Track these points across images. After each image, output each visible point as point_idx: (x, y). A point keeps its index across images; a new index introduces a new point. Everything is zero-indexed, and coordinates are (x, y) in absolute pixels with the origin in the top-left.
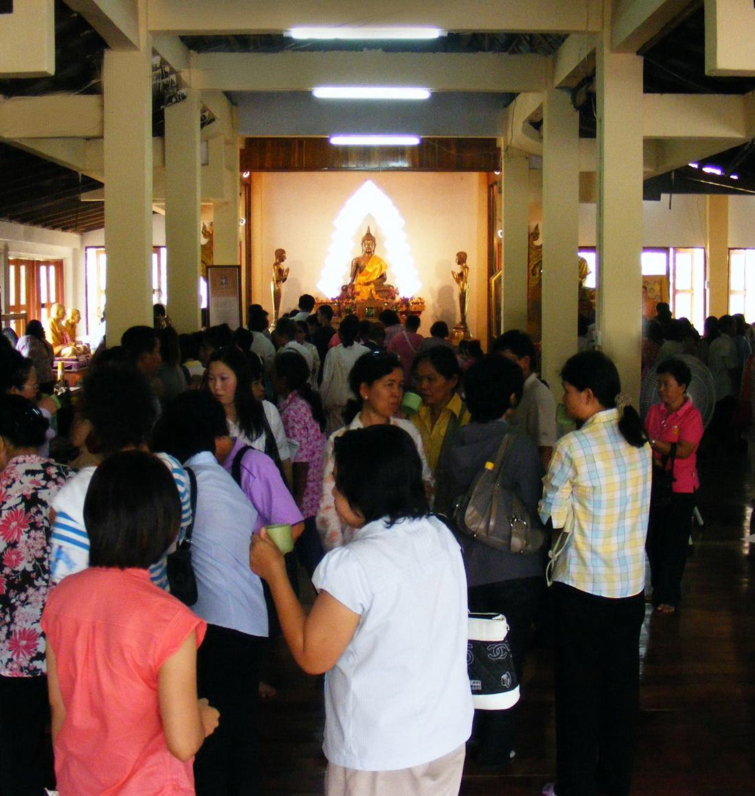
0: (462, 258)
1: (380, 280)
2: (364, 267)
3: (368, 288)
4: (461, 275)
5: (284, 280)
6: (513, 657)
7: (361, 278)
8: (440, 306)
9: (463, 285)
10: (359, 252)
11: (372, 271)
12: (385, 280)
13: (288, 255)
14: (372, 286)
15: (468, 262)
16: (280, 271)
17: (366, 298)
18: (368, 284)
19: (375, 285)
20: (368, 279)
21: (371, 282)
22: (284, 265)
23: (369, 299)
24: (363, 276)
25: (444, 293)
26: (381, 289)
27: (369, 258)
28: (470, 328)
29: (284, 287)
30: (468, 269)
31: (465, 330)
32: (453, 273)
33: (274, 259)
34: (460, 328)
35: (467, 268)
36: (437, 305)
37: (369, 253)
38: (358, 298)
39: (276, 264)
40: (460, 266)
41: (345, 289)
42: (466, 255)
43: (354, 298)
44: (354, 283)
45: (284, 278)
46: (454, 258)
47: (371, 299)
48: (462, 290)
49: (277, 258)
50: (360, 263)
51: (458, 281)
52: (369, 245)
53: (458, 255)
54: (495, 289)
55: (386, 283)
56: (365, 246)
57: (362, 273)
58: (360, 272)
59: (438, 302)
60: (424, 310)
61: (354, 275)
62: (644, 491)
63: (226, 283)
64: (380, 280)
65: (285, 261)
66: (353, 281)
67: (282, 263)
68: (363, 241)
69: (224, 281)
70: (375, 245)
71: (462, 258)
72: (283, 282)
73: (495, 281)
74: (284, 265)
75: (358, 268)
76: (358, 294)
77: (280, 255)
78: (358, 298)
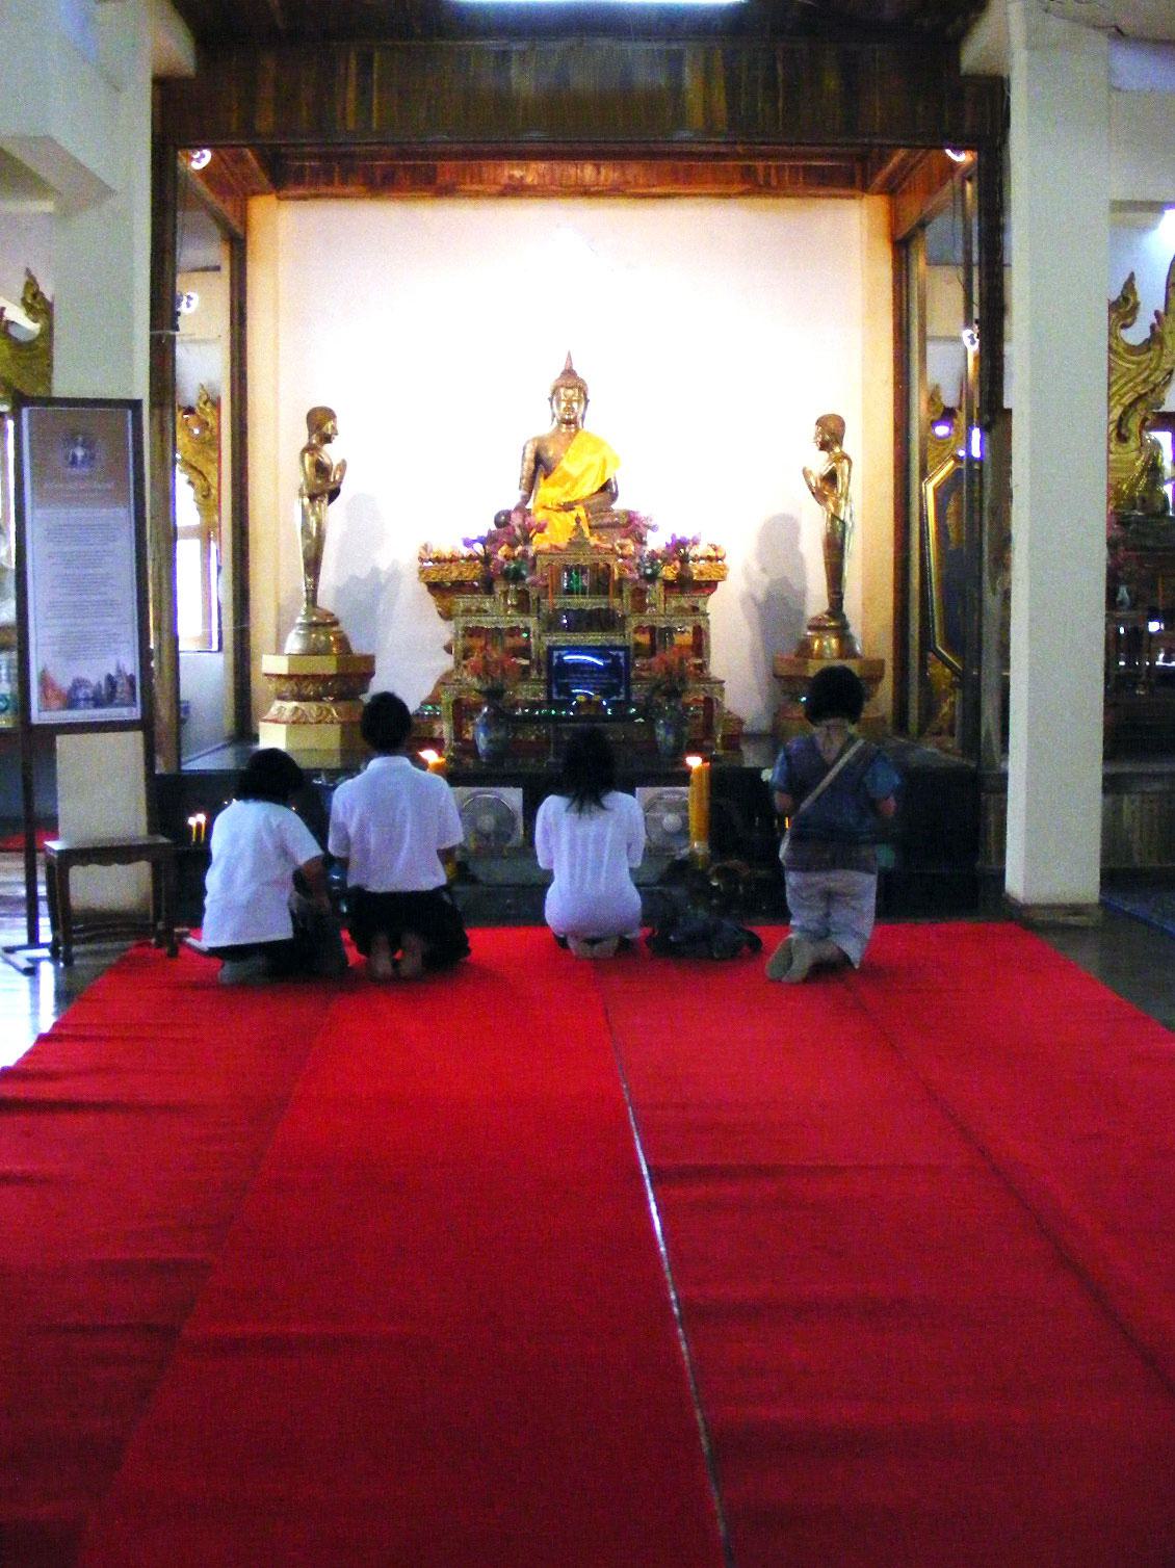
0: (831, 434)
1: (598, 499)
2: (558, 460)
3: (569, 519)
4: (831, 478)
5: (334, 494)
6: (677, 1297)
7: (548, 492)
8: (764, 570)
9: (837, 506)
10: (541, 422)
11: (579, 473)
12: (614, 497)
13: (344, 425)
14: (580, 511)
15: (851, 444)
16: (321, 469)
17: (562, 541)
18: (568, 507)
19: (587, 508)
20: (567, 493)
21: (576, 502)
22: (331, 454)
23: (571, 543)
24: (553, 485)
25: (779, 535)
26: (607, 520)
27: (572, 437)
28: (855, 630)
29: (335, 516)
30: (850, 462)
31: (842, 631)
32: (806, 474)
33: (302, 437)
34: (825, 629)
35: (845, 457)
36: (755, 567)
37: (568, 422)
38: (540, 542)
39: (310, 449)
40: (824, 455)
41: (503, 520)
42: (841, 423)
43: (527, 540)
44: (529, 506)
45: (332, 487)
46: (810, 432)
47: (577, 543)
48: (835, 517)
49: (311, 433)
50: (547, 451)
51: (819, 495)
52: (570, 402)
53: (819, 423)
54: (938, 532)
55: (618, 506)
56: (558, 405)
57: (551, 479)
58: (546, 477)
59: (760, 556)
60: (723, 578)
61: (531, 485)
62: (133, 609)
63: (90, 459)
64: (598, 499)
65: (336, 440)
66: (526, 500)
67: (327, 447)
68: (555, 391)
69: (80, 453)
70: (587, 401)
71: (831, 434)
72: (331, 500)
73: (936, 490)
74: (331, 454)
75: (541, 466)
76: (541, 529)
77: (320, 424)
78: (540, 542)
